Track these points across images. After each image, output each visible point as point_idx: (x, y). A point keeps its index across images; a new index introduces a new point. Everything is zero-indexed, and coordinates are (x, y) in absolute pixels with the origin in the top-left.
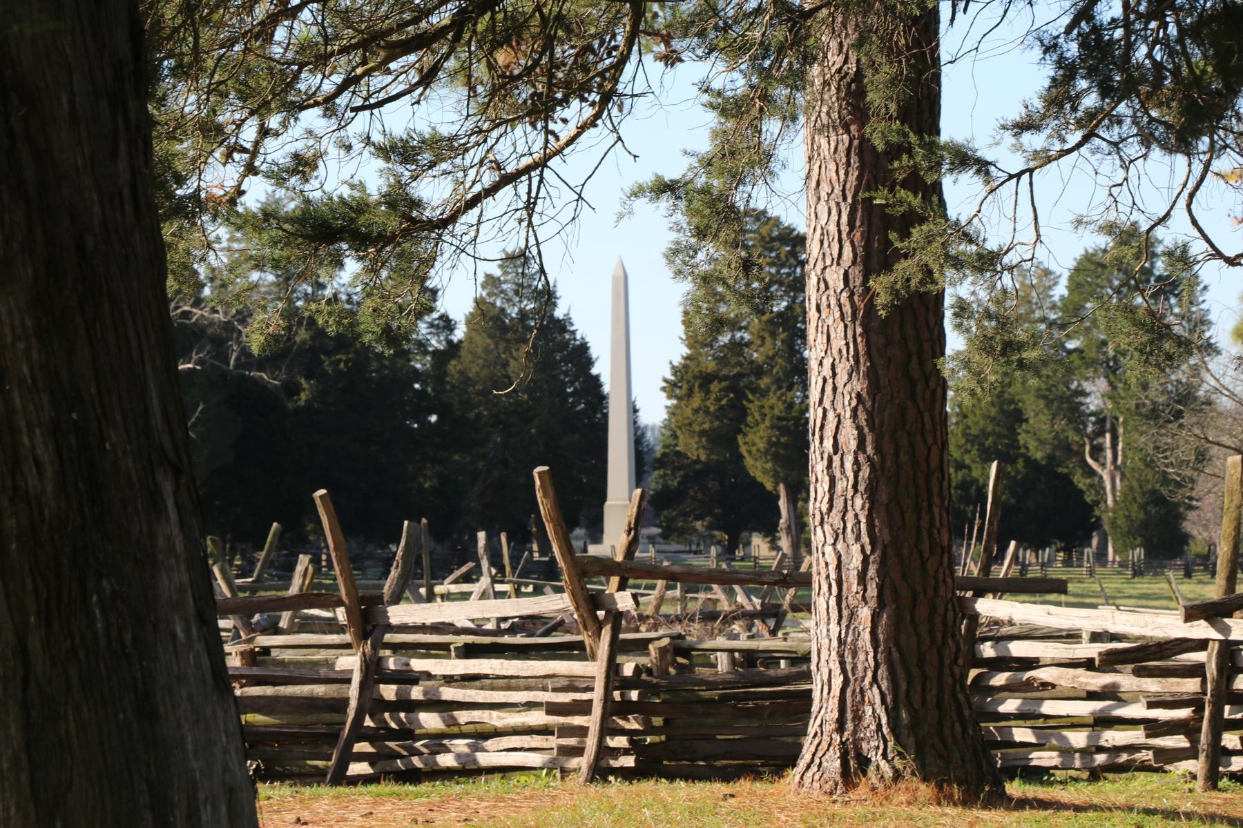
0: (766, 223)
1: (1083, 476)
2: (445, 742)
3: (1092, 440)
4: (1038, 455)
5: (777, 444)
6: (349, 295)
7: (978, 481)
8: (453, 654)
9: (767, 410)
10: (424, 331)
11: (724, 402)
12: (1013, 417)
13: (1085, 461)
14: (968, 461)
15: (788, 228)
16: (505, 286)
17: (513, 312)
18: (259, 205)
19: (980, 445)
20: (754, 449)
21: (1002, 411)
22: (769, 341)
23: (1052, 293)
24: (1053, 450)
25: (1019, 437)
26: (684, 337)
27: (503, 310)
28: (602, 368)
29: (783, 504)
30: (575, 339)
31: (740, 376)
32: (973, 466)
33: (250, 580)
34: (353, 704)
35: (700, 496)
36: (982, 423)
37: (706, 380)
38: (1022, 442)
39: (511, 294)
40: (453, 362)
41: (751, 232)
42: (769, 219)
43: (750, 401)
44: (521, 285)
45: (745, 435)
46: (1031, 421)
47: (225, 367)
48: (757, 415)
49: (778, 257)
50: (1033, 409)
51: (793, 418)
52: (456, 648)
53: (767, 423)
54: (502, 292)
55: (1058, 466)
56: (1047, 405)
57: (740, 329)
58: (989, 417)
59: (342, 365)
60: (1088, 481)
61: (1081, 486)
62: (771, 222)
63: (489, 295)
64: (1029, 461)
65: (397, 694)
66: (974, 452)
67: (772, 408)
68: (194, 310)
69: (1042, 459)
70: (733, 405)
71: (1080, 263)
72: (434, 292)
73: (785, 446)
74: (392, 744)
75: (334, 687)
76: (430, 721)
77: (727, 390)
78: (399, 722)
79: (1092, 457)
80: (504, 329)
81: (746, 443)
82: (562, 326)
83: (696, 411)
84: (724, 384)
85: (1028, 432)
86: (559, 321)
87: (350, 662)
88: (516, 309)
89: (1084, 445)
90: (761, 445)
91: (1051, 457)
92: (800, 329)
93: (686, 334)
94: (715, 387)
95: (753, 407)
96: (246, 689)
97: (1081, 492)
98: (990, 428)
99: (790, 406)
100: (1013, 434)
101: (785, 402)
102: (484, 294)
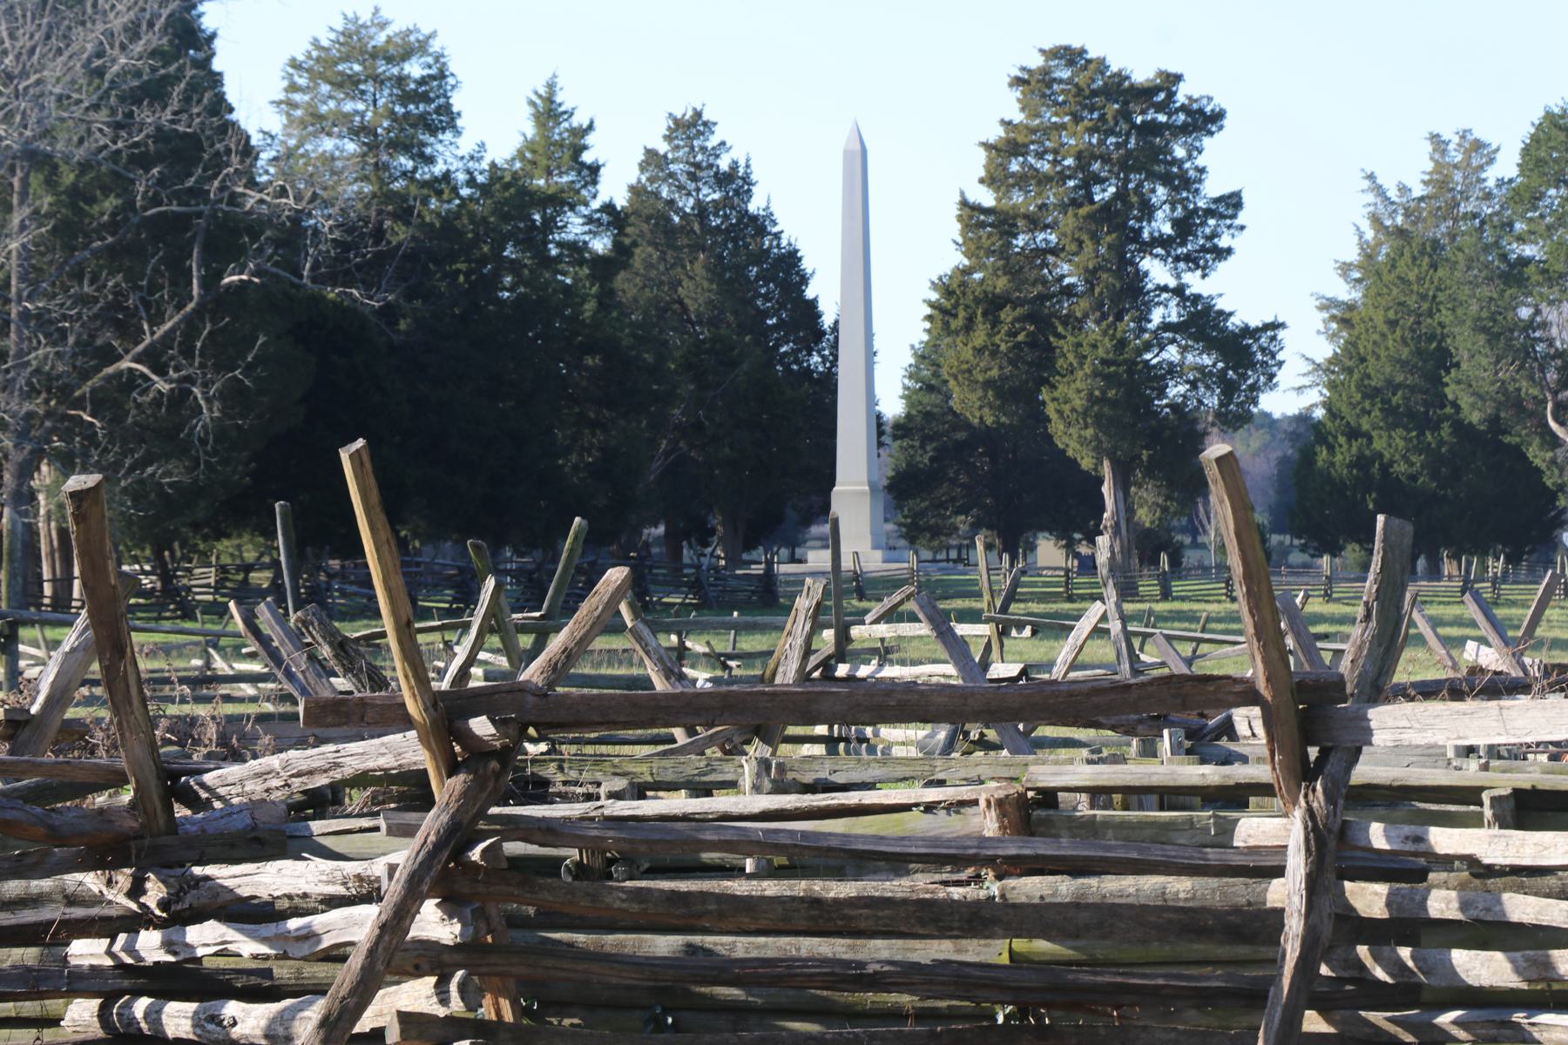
0: (1084, 68)
1: (1541, 448)
2: (1518, 1017)
3: (1555, 393)
4: (1476, 418)
5: (1103, 400)
6: (469, 172)
7: (1381, 456)
8: (1488, 813)
9: (1086, 350)
10: (578, 230)
11: (1021, 338)
12: (1435, 360)
13: (1546, 425)
14: (1366, 427)
15: (1119, 74)
16: (673, 167)
17: (688, 204)
18: (333, 36)
19: (1383, 402)
20: (1066, 408)
21: (1419, 352)
22: (1089, 246)
23: (1484, 175)
24: (1498, 409)
25: (1447, 390)
26: (960, 240)
27: (671, 203)
28: (826, 291)
29: (1107, 489)
30: (778, 246)
31: (1043, 298)
32: (1374, 433)
33: (537, 614)
34: (1294, 926)
35: (963, 478)
36: (1388, 370)
37: (993, 304)
38: (1450, 397)
39: (683, 178)
40: (622, 275)
41: (1061, 81)
42: (1089, 61)
43: (1060, 337)
44: (698, 166)
45: (1054, 387)
46: (1464, 366)
47: (296, 280)
48: (1071, 357)
49: (1102, 118)
50: (1465, 343)
51: (1126, 361)
52: (1493, 799)
53: (1088, 369)
54: (672, 175)
55: (1505, 432)
56: (1489, 341)
57: (1046, 227)
58: (1399, 361)
59: (461, 278)
60: (1549, 455)
61: (1537, 462)
62: (1092, 66)
63: (651, 180)
64: (1461, 428)
65: (1388, 904)
66: (1376, 413)
67: (1094, 346)
68: (248, 192)
69: (1480, 422)
70: (1032, 343)
71: (1539, 127)
72: (594, 170)
73: (1114, 404)
74: (1376, 1017)
75: (1213, 882)
76: (1483, 968)
77: (1029, 317)
78: (1397, 967)
79: (1556, 420)
80: (670, 232)
81: (1054, 399)
82: (759, 225)
83: (979, 351)
84: (1019, 311)
85: (1459, 382)
86: (754, 218)
87: (1272, 829)
88: (691, 201)
89: (1545, 401)
90: (1078, 403)
91: (1494, 421)
92: (1132, 229)
93: (963, 234)
94: (1007, 315)
95: (1066, 345)
96: (1011, 882)
97: (1538, 470)
98: (1400, 378)
99: (1122, 344)
100: (1438, 382)
101: (1113, 337)
102: (644, 179)
